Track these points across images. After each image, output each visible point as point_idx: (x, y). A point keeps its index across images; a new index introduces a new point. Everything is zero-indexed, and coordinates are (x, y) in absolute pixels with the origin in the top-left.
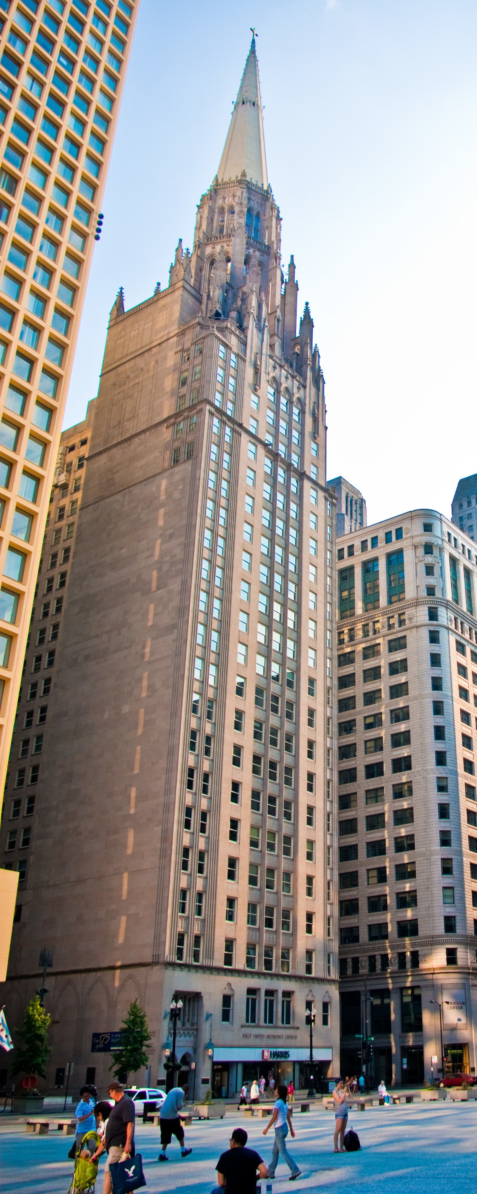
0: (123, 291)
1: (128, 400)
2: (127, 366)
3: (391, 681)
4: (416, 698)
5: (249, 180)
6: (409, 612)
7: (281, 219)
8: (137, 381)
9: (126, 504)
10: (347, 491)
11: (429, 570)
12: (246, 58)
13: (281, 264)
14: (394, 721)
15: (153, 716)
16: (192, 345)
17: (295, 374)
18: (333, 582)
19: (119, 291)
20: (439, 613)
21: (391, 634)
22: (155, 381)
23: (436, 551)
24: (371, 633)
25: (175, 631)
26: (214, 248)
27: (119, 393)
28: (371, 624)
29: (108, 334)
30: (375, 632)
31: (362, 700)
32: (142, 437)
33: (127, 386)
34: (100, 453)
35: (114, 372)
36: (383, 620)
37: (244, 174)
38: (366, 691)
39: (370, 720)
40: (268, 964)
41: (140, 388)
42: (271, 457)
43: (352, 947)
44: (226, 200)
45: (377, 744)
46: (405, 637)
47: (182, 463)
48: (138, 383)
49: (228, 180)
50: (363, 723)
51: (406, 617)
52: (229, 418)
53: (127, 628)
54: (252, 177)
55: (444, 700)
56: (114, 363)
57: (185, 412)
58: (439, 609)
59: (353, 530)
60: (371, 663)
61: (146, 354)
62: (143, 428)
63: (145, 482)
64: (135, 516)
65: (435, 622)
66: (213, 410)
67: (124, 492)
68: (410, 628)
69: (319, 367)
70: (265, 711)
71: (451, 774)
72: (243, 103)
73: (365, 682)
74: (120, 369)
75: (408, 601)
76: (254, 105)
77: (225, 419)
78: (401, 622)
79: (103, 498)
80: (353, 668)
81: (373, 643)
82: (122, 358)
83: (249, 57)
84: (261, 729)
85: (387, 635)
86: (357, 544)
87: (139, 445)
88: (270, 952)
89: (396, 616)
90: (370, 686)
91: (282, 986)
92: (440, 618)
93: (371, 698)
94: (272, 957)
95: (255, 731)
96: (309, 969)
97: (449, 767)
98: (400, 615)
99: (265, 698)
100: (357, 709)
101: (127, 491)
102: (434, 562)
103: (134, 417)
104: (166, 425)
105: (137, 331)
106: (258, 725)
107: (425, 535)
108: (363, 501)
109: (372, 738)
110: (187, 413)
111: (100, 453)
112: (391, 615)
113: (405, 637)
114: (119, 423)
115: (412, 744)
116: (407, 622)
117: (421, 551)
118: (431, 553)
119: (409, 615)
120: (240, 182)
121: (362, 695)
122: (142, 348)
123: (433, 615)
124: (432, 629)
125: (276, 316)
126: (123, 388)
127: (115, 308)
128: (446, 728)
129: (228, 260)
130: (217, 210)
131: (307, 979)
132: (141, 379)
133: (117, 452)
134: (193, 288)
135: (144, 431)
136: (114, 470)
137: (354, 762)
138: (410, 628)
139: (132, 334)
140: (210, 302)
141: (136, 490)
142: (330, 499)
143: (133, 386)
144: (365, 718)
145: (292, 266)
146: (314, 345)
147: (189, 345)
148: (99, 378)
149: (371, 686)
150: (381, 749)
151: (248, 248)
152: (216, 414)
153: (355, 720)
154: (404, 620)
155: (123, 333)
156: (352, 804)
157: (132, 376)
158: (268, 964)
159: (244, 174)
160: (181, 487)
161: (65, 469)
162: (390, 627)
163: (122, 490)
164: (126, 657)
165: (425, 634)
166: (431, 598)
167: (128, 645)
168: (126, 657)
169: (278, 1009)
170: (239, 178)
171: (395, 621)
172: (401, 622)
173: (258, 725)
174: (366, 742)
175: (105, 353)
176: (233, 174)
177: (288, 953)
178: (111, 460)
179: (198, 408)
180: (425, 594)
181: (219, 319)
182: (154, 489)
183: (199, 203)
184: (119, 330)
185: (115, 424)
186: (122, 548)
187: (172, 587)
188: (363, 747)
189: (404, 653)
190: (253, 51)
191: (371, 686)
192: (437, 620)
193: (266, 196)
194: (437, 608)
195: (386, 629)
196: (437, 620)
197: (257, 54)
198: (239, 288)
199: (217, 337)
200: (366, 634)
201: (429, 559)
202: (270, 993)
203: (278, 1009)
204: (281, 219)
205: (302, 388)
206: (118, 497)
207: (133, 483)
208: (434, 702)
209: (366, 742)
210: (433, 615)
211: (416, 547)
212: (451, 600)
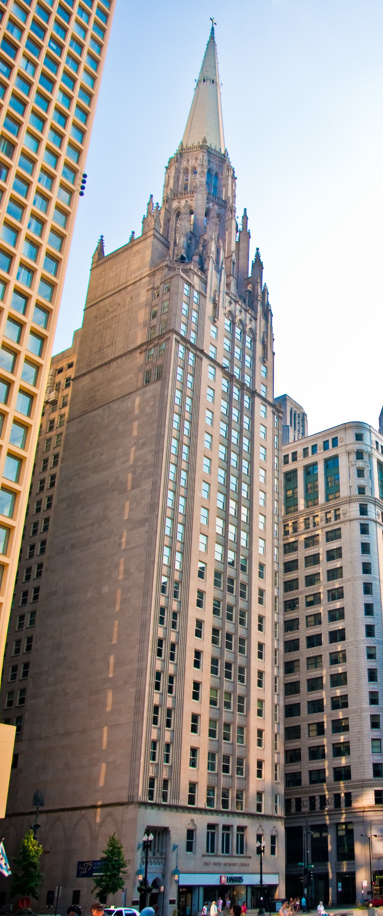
0: (103, 239)
1: (108, 330)
3: (328, 566)
4: (349, 580)
6: (343, 508)
7: (236, 178)
8: (115, 314)
9: (106, 417)
11: (360, 473)
12: (207, 43)
13: (236, 216)
14: (330, 599)
16: (161, 284)
18: (279, 482)
20: (369, 509)
23: (366, 457)
24: (311, 526)
25: (147, 524)
26: (179, 202)
27: (100, 324)
28: (311, 518)
29: (91, 275)
30: (315, 525)
31: (304, 582)
32: (119, 361)
33: (106, 319)
34: (84, 375)
35: (96, 306)
36: (321, 514)
37: (205, 141)
40: (225, 804)
41: (117, 320)
42: (228, 378)
43: (295, 789)
44: (190, 163)
45: (317, 619)
46: (340, 529)
47: (153, 383)
48: (116, 316)
49: (191, 145)
50: (304, 601)
51: (341, 512)
52: (192, 345)
53: (106, 521)
54: (211, 142)
55: (373, 582)
56: (96, 299)
57: (155, 340)
58: (369, 506)
59: (296, 439)
60: (311, 551)
61: (123, 292)
62: (120, 353)
63: (122, 399)
65: (365, 517)
66: (179, 338)
69: (268, 302)
70: (223, 591)
71: (379, 644)
72: (204, 81)
75: (343, 499)
76: (213, 82)
77: (188, 346)
78: (337, 517)
80: (296, 555)
81: (313, 534)
84: (219, 607)
85: (325, 527)
86: (300, 451)
87: (117, 368)
88: (227, 794)
89: (333, 512)
92: (369, 513)
93: (311, 580)
94: (228, 798)
95: (214, 608)
97: (377, 638)
100: (300, 589)
101: (107, 406)
102: (364, 466)
103: (112, 344)
105: (115, 273)
106: (217, 603)
107: (357, 444)
109: (312, 613)
111: (84, 375)
112: (329, 510)
113: (340, 529)
115: (345, 619)
116: (342, 516)
117: (353, 457)
119: (343, 511)
120: (201, 147)
121: (304, 577)
123: (363, 511)
125: (232, 260)
126: (103, 320)
127: (97, 253)
129: (192, 213)
130: (182, 171)
132: (118, 312)
133: (98, 374)
134: (162, 236)
135: (121, 356)
140: (176, 248)
143: (112, 318)
144: (306, 597)
145: (245, 218)
146: (263, 284)
147: (159, 284)
150: (320, 623)
152: (182, 342)
153: (298, 599)
154: (339, 515)
155: (103, 274)
156: (296, 669)
157: (111, 310)
158: (225, 804)
159: (205, 141)
160: (152, 403)
161: (55, 388)
162: (328, 520)
165: (356, 526)
168: (105, 545)
170: (201, 144)
171: (331, 515)
172: (337, 517)
175: (88, 291)
176: (195, 141)
177: (242, 794)
178: (93, 380)
179: (166, 337)
180: (357, 493)
181: (184, 262)
182: (129, 405)
183: (167, 165)
184: (100, 271)
186: (102, 455)
187: (144, 487)
189: (339, 543)
190: (212, 37)
191: (312, 570)
192: (367, 515)
193: (223, 159)
194: (366, 505)
195: (324, 522)
196: (367, 515)
199: (182, 277)
200: (307, 527)
202: (226, 828)
204: (236, 178)
205: (253, 320)
206: (99, 411)
207: (112, 400)
208: (364, 584)
210: (363, 511)
211: (349, 454)
212: (378, 498)
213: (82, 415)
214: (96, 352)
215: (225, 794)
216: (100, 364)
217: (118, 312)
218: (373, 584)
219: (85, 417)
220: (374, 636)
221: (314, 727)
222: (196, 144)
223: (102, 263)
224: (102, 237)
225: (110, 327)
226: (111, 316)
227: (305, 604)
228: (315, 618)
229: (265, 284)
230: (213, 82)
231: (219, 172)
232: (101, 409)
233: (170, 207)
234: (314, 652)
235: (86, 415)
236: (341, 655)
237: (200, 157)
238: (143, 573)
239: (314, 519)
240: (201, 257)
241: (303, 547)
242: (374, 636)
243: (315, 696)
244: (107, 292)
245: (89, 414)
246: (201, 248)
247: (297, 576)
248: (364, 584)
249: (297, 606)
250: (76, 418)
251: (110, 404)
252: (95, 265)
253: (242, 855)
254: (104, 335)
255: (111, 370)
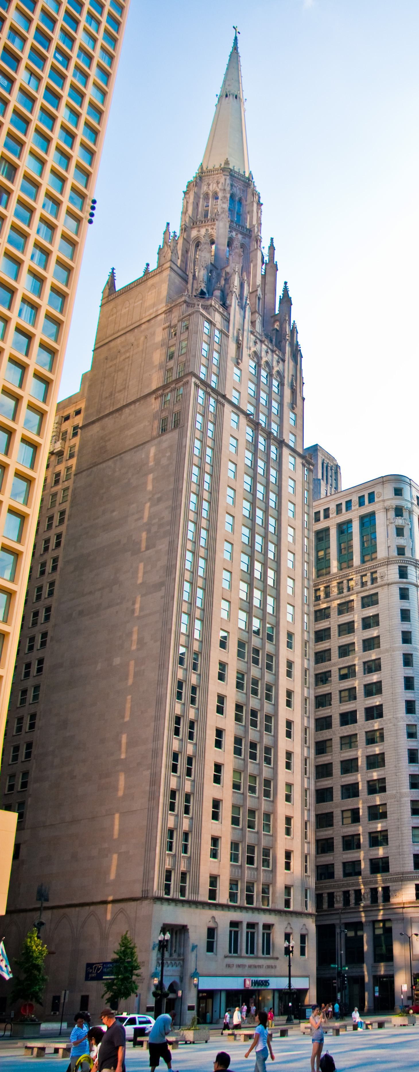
0: (115, 271)
1: (120, 373)
2: (119, 341)
3: (364, 635)
4: (387, 651)
5: (232, 168)
7: (262, 204)
8: (128, 355)
9: (117, 470)
10: (323, 457)
13: (262, 246)
14: (366, 672)
15: (143, 667)
16: (178, 321)
17: (275, 348)
18: (310, 542)
19: (111, 271)
20: (409, 571)
21: (364, 591)
22: (144, 355)
23: (406, 514)
24: (345, 590)
25: (163, 588)
26: (199, 231)
27: (111, 367)
28: (345, 582)
30: (349, 589)
31: (337, 652)
32: (132, 407)
33: (118, 360)
34: (93, 422)
36: (356, 578)
37: (227, 163)
38: (341, 644)
39: (344, 672)
40: (250, 899)
42: (253, 426)
44: (211, 187)
45: (351, 694)
47: (170, 432)
48: (129, 357)
49: (212, 168)
50: (337, 674)
51: (378, 575)
52: (213, 390)
54: (234, 165)
55: (413, 653)
56: (106, 338)
57: (172, 384)
58: (409, 568)
59: (329, 494)
60: (345, 619)
61: (136, 330)
62: (133, 399)
63: (135, 449)
64: (126, 481)
65: (405, 580)
66: (198, 382)
67: (115, 459)
68: (382, 586)
69: (297, 342)
70: (247, 663)
72: (227, 96)
73: (339, 636)
74: (112, 344)
77: (209, 390)
78: (374, 580)
79: (96, 464)
80: (328, 623)
81: (347, 599)
82: (114, 334)
83: (232, 53)
84: (243, 680)
85: (361, 592)
86: (333, 507)
87: (130, 415)
88: (251, 888)
89: (369, 574)
90: (344, 640)
91: (263, 919)
92: (409, 576)
93: (345, 650)
95: (237, 681)
96: (287, 903)
98: (372, 573)
99: (246, 651)
100: (333, 661)
101: (118, 457)
102: (404, 524)
103: (125, 388)
104: (154, 396)
105: (127, 309)
108: (337, 467)
109: (346, 688)
110: (174, 385)
111: (93, 422)
112: (364, 573)
113: (377, 594)
114: (111, 394)
116: (379, 580)
117: (392, 514)
118: (402, 515)
119: (380, 573)
120: (223, 170)
121: (337, 648)
122: (132, 324)
124: (402, 586)
125: (257, 295)
126: (115, 362)
128: (415, 678)
129: (212, 242)
130: (202, 196)
131: (286, 912)
132: (131, 353)
134: (180, 268)
135: (134, 402)
136: (107, 439)
137: (329, 710)
138: (382, 586)
139: (123, 312)
140: (195, 282)
141: (127, 457)
142: (307, 465)
143: (124, 360)
144: (340, 669)
146: (292, 322)
147: (176, 321)
148: (92, 353)
149: (346, 640)
150: (355, 698)
151: (231, 232)
152: (201, 386)
153: (330, 671)
154: (376, 578)
156: (328, 749)
158: (250, 899)
159: (227, 163)
160: (168, 454)
162: (363, 584)
163: (114, 457)
164: (117, 612)
165: (395, 591)
166: (401, 558)
167: (119, 601)
168: (117, 612)
169: (259, 941)
170: (222, 166)
172: (374, 580)
173: (240, 676)
174: (340, 691)
175: (98, 329)
176: (217, 162)
178: (103, 429)
179: (185, 380)
180: (395, 553)
181: (204, 298)
182: (143, 456)
183: (185, 190)
184: (111, 307)
185: (107, 395)
186: (113, 511)
188: (338, 697)
189: (376, 609)
190: (235, 48)
191: (346, 640)
192: (407, 578)
193: (247, 183)
194: (406, 567)
195: (360, 586)
196: (407, 578)
197: (239, 50)
198: (223, 269)
199: (202, 314)
200: (340, 591)
201: (399, 521)
202: (251, 926)
203: (259, 941)
204: (262, 204)
205: (281, 362)
206: (110, 463)
208: (404, 654)
209: (340, 691)
211: (387, 510)
213: (91, 468)
214: (106, 398)
215: (250, 888)
216: (111, 410)
217: (131, 353)
218: (414, 655)
219: (95, 469)
220: (415, 713)
221: (349, 814)
222: (217, 166)
223: (113, 299)
224: (113, 269)
225: (122, 370)
226: (123, 357)
227: (338, 677)
228: (349, 693)
229: (294, 321)
230: (236, 97)
231: (243, 198)
232: (112, 460)
233: (189, 236)
234: (348, 730)
235: (96, 467)
236: (378, 734)
237: (222, 180)
238: (159, 643)
239: (348, 583)
240: (223, 291)
241: (337, 614)
242: (415, 713)
243: (349, 779)
244: (118, 331)
245: (99, 466)
246: (223, 282)
247: (330, 646)
248: (404, 654)
249: (329, 679)
250: (84, 471)
251: (122, 455)
252: (105, 300)
253: (268, 956)
254: (115, 378)
255: (123, 417)
